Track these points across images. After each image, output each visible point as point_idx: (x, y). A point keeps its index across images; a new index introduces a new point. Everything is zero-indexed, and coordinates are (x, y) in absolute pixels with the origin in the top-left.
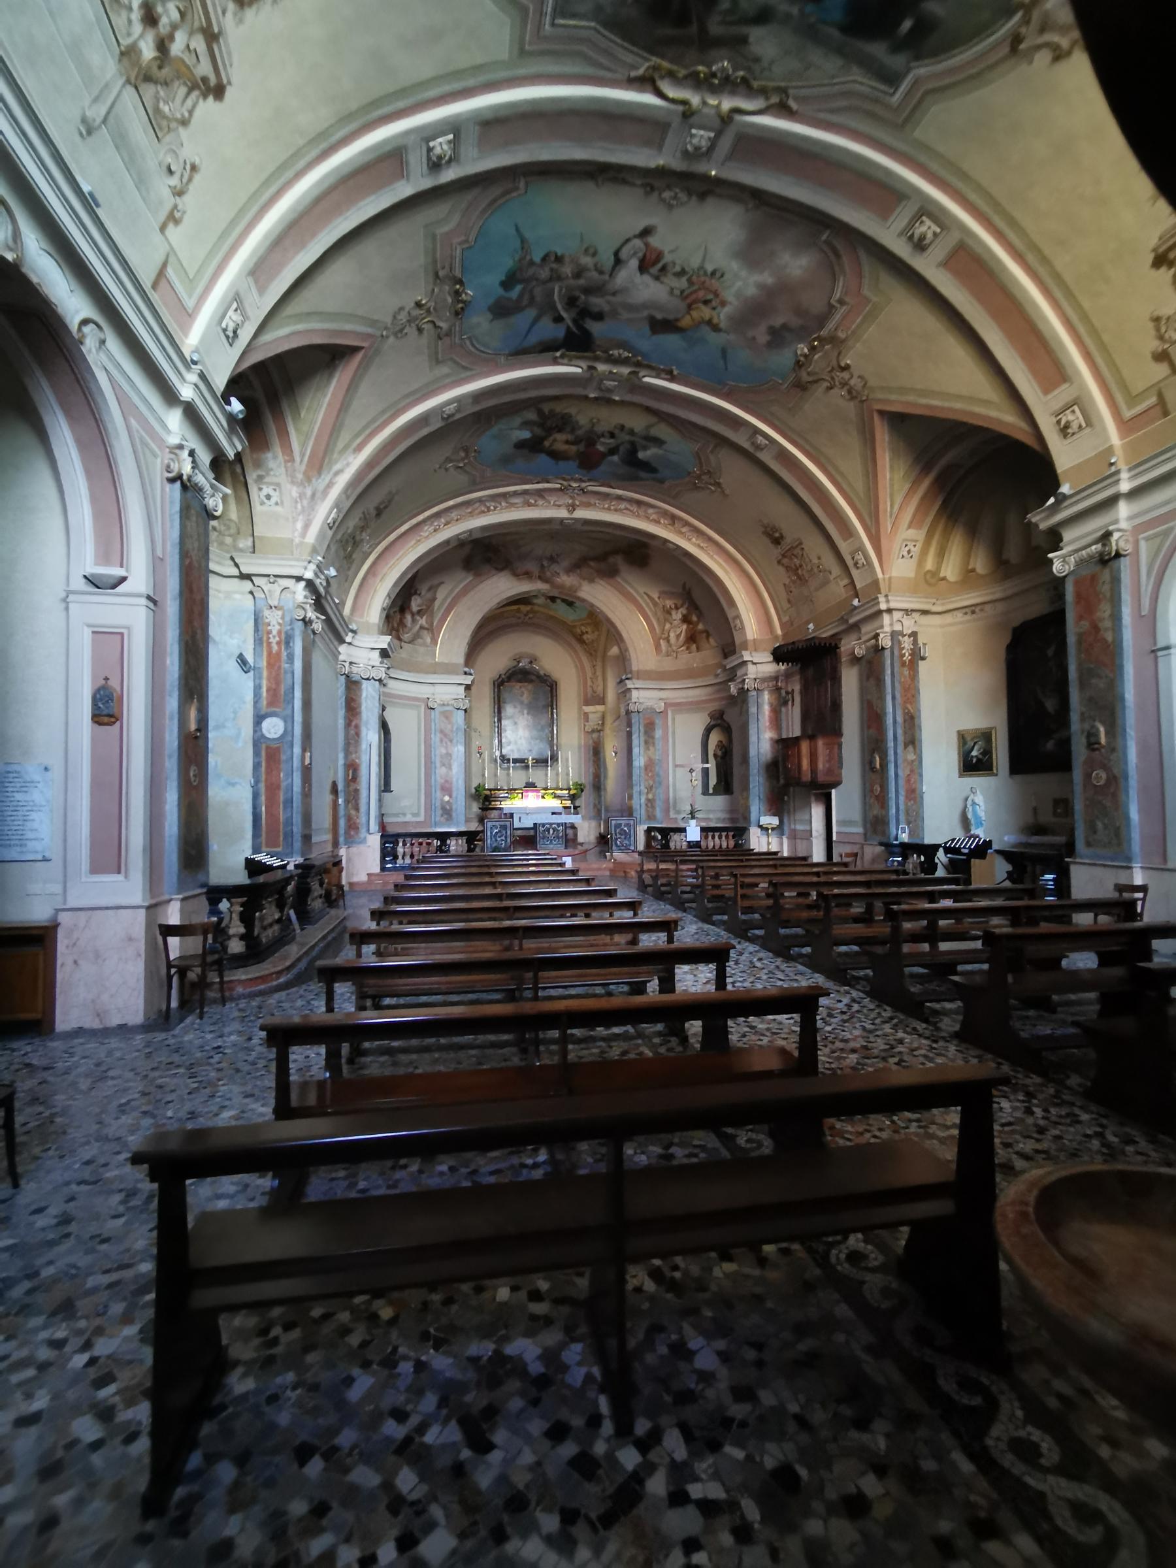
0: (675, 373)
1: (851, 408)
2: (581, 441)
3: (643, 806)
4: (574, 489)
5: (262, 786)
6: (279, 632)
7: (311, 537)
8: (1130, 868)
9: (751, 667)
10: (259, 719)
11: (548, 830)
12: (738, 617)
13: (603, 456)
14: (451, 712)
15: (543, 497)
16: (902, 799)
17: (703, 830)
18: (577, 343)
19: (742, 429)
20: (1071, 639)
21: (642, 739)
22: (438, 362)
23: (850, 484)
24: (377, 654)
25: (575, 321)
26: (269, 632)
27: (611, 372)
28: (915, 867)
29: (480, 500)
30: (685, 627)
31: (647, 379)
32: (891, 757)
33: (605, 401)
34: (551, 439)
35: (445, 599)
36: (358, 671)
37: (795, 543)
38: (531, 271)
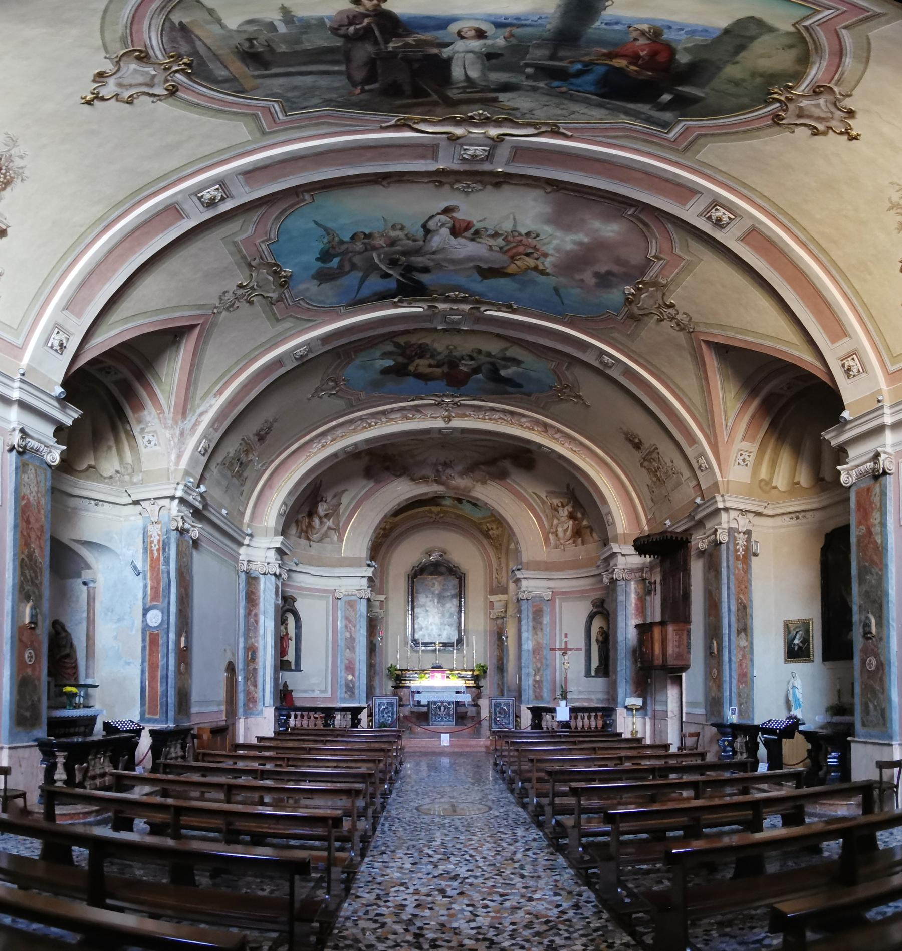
0: (515, 306)
2: (443, 364)
4: (448, 404)
5: (146, 665)
6: (159, 541)
7: (183, 464)
8: (892, 745)
9: (620, 558)
10: (146, 611)
11: (440, 708)
12: (610, 513)
13: (467, 376)
14: (355, 601)
15: (418, 411)
16: (734, 682)
18: (410, 289)
20: (853, 540)
21: (531, 624)
25: (401, 275)
26: (152, 542)
27: (451, 309)
28: (741, 746)
29: (361, 419)
32: (726, 643)
33: (453, 330)
34: (415, 363)
35: (350, 502)
36: (257, 568)
37: (650, 449)
38: (344, 247)
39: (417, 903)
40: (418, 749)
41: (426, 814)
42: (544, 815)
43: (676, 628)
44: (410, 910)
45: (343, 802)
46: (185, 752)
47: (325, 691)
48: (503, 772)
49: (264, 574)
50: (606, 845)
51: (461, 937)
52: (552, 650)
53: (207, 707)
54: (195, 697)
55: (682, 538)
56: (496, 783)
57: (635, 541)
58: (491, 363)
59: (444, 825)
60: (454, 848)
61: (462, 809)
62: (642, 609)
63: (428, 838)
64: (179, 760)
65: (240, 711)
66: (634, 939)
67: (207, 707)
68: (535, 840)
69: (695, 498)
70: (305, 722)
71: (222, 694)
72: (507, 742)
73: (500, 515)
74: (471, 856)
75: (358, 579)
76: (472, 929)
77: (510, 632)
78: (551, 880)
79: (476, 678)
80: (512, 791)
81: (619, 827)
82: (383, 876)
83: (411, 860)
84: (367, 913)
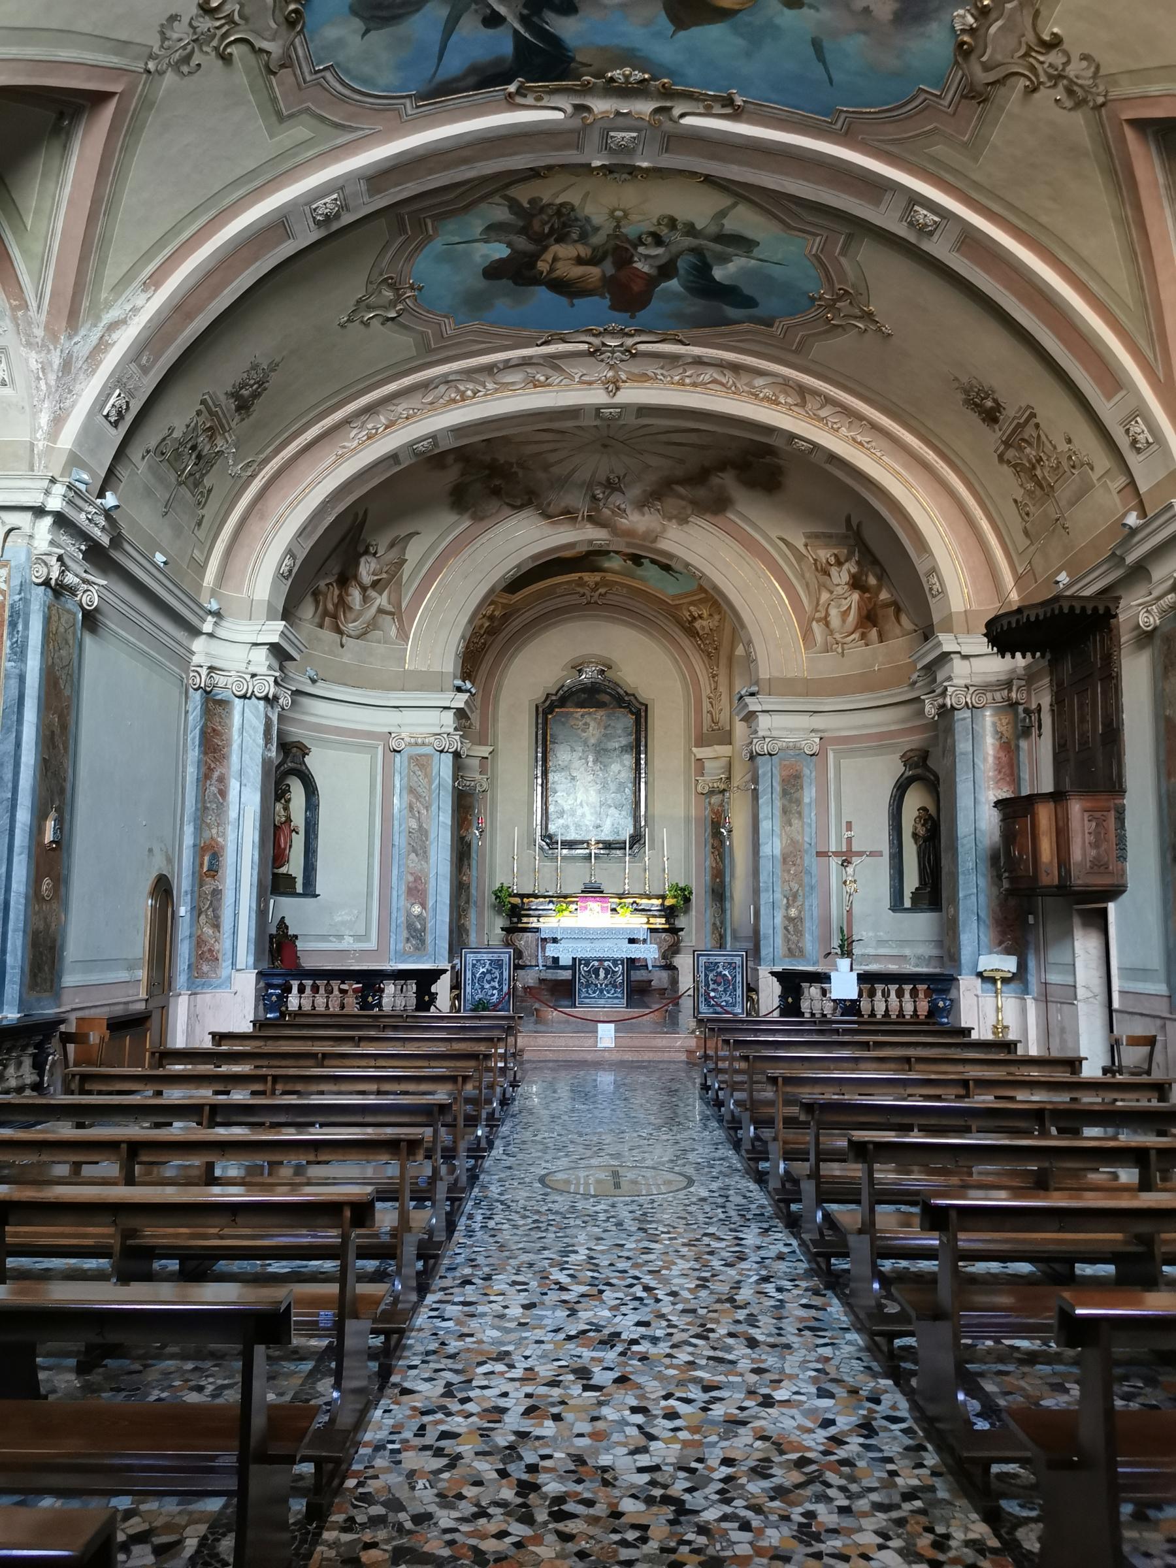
0: (739, 101)
1: (1078, 122)
3: (780, 932)
9: (957, 662)
11: (596, 971)
12: (934, 570)
13: (652, 282)
14: (431, 756)
15: (556, 368)
17: (863, 978)
19: (888, 196)
21: (778, 804)
22: (281, 118)
23: (1104, 282)
24: (261, 655)
29: (446, 380)
30: (856, 596)
31: (688, 121)
34: (548, 256)
35: (421, 563)
39: (529, 1402)
40: (550, 1056)
41: (561, 1192)
42: (799, 1201)
43: (1088, 805)
44: (514, 1420)
45: (389, 1169)
46: (41, 1075)
47: (366, 937)
48: (719, 1104)
49: (244, 697)
50: (920, 1278)
51: (617, 1492)
52: (819, 854)
53: (101, 967)
54: (74, 949)
55: (1095, 609)
56: (705, 1127)
57: (989, 625)
58: (692, 250)
59: (594, 1216)
60: (613, 1280)
61: (634, 1182)
62: (1010, 765)
63: (560, 1246)
64: (28, 1092)
65: (181, 979)
66: (998, 1535)
67: (101, 967)
68: (780, 1257)
69: (1125, 515)
70: (320, 1000)
71: (139, 944)
72: (727, 1042)
73: (715, 588)
74: (647, 1289)
75: (437, 712)
76: (641, 1470)
77: (738, 820)
78: (813, 1356)
79: (669, 913)
80: (737, 1145)
81: (956, 1240)
82: (462, 1336)
83: (523, 1298)
84: (421, 1430)
